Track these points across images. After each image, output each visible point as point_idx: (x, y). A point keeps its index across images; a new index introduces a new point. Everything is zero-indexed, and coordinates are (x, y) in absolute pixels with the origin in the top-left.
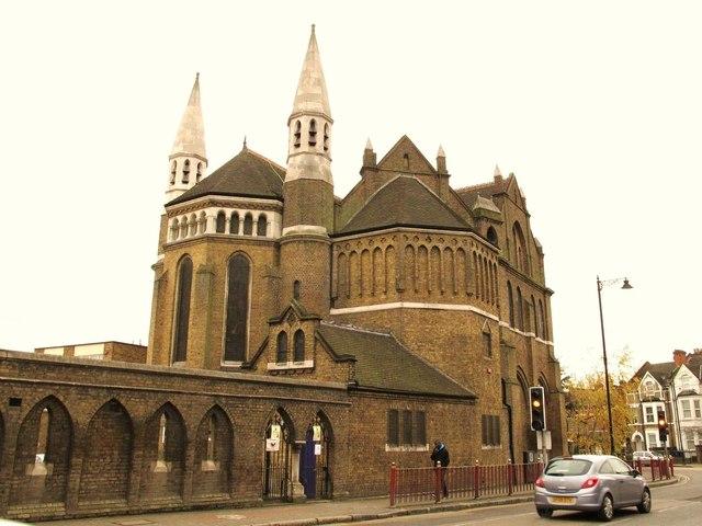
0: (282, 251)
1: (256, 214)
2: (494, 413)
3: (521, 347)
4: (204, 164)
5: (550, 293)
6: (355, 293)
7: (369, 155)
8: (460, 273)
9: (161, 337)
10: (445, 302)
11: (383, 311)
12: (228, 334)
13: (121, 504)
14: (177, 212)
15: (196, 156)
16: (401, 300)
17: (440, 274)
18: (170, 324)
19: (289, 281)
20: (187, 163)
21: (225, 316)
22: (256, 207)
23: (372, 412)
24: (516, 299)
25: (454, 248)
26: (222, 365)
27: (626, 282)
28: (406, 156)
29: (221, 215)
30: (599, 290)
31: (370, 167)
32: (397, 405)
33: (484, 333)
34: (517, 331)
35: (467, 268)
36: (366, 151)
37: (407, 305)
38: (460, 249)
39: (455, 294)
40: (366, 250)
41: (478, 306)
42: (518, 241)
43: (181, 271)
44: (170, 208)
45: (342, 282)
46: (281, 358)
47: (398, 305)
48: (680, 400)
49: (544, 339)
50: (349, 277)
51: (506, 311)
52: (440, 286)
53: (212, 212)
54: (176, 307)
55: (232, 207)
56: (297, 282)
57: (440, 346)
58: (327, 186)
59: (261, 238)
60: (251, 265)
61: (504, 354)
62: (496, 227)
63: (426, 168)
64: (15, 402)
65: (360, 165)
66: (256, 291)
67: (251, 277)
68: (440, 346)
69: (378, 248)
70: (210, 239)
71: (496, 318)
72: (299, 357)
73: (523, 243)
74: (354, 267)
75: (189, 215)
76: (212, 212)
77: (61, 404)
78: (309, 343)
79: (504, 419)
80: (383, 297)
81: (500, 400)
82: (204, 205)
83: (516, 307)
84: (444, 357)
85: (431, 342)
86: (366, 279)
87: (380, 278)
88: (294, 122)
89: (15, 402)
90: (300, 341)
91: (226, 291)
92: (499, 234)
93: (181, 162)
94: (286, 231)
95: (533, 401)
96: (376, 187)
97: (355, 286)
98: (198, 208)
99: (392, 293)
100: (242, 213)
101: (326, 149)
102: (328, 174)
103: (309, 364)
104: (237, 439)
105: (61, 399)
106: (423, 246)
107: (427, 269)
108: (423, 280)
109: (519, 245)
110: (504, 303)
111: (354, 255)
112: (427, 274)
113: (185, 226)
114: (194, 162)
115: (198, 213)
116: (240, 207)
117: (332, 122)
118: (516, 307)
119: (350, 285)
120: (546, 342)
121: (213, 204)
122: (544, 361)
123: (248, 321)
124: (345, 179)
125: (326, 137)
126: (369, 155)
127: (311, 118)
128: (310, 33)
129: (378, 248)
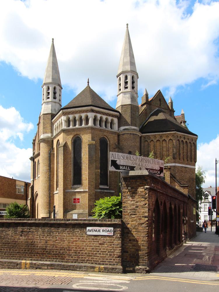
16: (175, 162)
30: (216, 164)
37: (177, 165)
40: (158, 140)
47: (173, 164)
53: (91, 115)
55: (100, 114)
60: (108, 143)
63: (166, 107)
69: (164, 140)
70: (92, 128)
76: (91, 115)
82: (87, 111)
85: (184, 180)
93: (122, 77)
94: (122, 128)
96: (150, 112)
101: (60, 100)
116: (104, 115)
121: (93, 111)
127: (47, 85)
128: (51, 43)
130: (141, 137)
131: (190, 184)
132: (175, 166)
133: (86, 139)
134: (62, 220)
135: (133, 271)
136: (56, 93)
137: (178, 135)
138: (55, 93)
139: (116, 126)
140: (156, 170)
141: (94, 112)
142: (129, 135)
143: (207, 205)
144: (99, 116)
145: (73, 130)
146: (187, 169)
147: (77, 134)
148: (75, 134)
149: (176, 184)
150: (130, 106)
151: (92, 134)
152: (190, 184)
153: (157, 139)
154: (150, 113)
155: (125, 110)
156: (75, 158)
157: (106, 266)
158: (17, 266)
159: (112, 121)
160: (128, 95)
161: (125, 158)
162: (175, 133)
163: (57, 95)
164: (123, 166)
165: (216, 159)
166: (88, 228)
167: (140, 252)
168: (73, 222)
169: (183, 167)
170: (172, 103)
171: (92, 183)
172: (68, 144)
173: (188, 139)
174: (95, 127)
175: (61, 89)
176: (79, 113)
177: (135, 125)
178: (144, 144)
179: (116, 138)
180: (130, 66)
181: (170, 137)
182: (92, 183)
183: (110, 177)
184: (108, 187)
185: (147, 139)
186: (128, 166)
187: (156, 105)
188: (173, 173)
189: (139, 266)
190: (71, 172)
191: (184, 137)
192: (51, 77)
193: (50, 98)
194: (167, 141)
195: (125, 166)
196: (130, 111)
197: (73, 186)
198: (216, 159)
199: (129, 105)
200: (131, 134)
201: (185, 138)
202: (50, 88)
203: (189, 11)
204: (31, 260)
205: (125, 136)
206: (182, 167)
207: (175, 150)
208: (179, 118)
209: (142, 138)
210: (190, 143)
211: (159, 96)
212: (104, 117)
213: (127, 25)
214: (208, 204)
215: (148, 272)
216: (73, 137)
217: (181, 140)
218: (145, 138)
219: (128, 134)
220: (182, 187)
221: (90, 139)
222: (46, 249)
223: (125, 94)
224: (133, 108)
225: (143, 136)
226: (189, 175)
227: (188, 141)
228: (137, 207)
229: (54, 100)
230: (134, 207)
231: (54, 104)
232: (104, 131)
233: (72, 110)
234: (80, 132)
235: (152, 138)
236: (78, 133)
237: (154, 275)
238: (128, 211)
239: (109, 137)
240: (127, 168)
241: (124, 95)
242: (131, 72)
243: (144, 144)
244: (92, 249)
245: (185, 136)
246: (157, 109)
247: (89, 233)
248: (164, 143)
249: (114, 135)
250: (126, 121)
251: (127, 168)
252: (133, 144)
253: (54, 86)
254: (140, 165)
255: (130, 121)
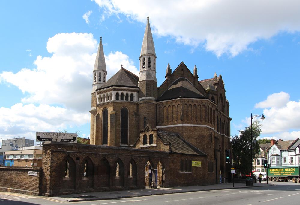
0: (139, 106)
1: (130, 93)
2: (212, 161)
3: (220, 139)
4: (106, 73)
5: (231, 119)
6: (165, 121)
7: (169, 70)
8: (203, 114)
9: (98, 136)
10: (197, 124)
11: (176, 127)
12: (121, 135)
13: (108, 188)
14: (101, 93)
15: (103, 71)
16: (183, 123)
17: (196, 114)
18: (101, 132)
19: (142, 117)
20: (100, 73)
21: (120, 129)
22: (129, 91)
23: (176, 161)
24: (219, 122)
25: (201, 105)
26: (120, 145)
27: (263, 116)
28: (183, 70)
29: (117, 94)
30: (252, 119)
31: (169, 74)
32: (183, 158)
33: (210, 134)
34: (219, 133)
35: (206, 112)
36: (168, 68)
37: (184, 125)
38: (204, 105)
39: (201, 121)
40: (169, 106)
41: (210, 126)
42: (221, 101)
43: (103, 113)
44: (98, 91)
45: (161, 117)
46: (145, 143)
47: (181, 125)
48: (271, 157)
49: (227, 136)
50: (163, 116)
51: (216, 127)
52: (196, 119)
53: (114, 93)
54: (102, 126)
56: (145, 117)
57: (195, 139)
58: (155, 83)
59: (132, 102)
60: (129, 111)
61: (216, 142)
62: (215, 96)
64: (78, 159)
65: (165, 74)
66: (130, 120)
67: (129, 117)
68: (195, 139)
69: (174, 105)
70: (114, 102)
71: (214, 129)
72: (151, 143)
73: (222, 102)
74: (165, 111)
75: (105, 94)
76: (114, 93)
77: (90, 159)
78: (155, 138)
79: (215, 163)
80: (176, 122)
81: (214, 157)
82: (111, 90)
83: (219, 125)
84: (196, 142)
86: (170, 116)
87: (175, 116)
88: (142, 59)
89: (78, 159)
90: (152, 138)
91: (120, 120)
92: (215, 99)
94: (140, 99)
95: (227, 157)
97: (165, 118)
98: (109, 91)
99: (180, 121)
100: (125, 93)
102: (155, 78)
103: (155, 145)
104: (138, 169)
105: (90, 157)
106: (195, 105)
107: (191, 112)
108: (190, 117)
109: (221, 102)
110: (216, 124)
111: (165, 108)
112: (192, 114)
113: (104, 98)
114: (102, 73)
115: (109, 93)
117: (156, 57)
118: (219, 125)
119: (164, 118)
120: (228, 137)
121: (114, 90)
122: (227, 143)
123: (128, 131)
124: (161, 79)
125: (154, 64)
126: (169, 70)
129: (174, 105)
130: (157, 104)
131: (200, 140)
132: (182, 127)
133: (110, 110)
134: (32, 168)
135: (44, 196)
136: (151, 62)
137: (185, 100)
138: (149, 62)
139: (135, 99)
140: (70, 140)
141: (116, 90)
142: (144, 104)
143: (275, 158)
144: (120, 92)
145: (103, 104)
146: (196, 128)
147: (105, 108)
148: (104, 107)
149: (161, 142)
150: (146, 82)
151: (114, 106)
152: (200, 140)
153: (169, 105)
154: (171, 83)
155: (142, 85)
156: (104, 124)
157: (33, 192)
158: (6, 191)
159: (132, 95)
160: (145, 73)
161: (46, 135)
162: (182, 99)
163: (152, 64)
164: (44, 139)
165: (252, 115)
166: (29, 172)
167: (47, 185)
168: (14, 168)
169: (192, 126)
170: (196, 71)
171: (113, 143)
172: (100, 115)
173: (197, 102)
174: (117, 101)
175: (106, 73)
176: (107, 92)
177: (150, 95)
178: (159, 110)
179: (135, 107)
180: (146, 50)
181: (179, 103)
182: (113, 143)
183: (129, 137)
184: (128, 145)
185: (161, 106)
186: (47, 139)
187: (179, 75)
188: (181, 132)
189: (47, 192)
190: (101, 135)
191: (193, 101)
192: (97, 66)
193: (97, 81)
194: (176, 106)
195: (46, 139)
196: (145, 86)
197: (103, 144)
198: (252, 115)
199: (146, 80)
200: (146, 103)
201: (193, 102)
202: (146, 59)
203: (36, 67)
204: (11, 188)
205: (142, 105)
206: (190, 126)
207: (182, 113)
208: (205, 82)
209: (158, 105)
210: (199, 105)
211: (182, 67)
212: (125, 93)
213: (101, 38)
214: (275, 157)
215: (50, 196)
216: (103, 110)
217: (188, 104)
218: (160, 105)
219: (144, 103)
220: (165, 144)
221: (113, 111)
222: (16, 182)
223: (143, 73)
224: (151, 83)
225: (158, 103)
226: (199, 133)
227: (197, 104)
228: (47, 161)
229: (100, 82)
230: (46, 161)
231: (99, 85)
232: (125, 103)
233: (102, 90)
234: (107, 106)
235: (165, 104)
236: (105, 106)
237: (51, 198)
238: (44, 163)
239: (129, 107)
240: (47, 140)
241: (142, 73)
242: (147, 55)
243: (159, 110)
244: (30, 183)
245: (194, 100)
246: (179, 78)
247: (29, 174)
248: (174, 107)
249: (133, 105)
250: (143, 93)
251: (47, 140)
252: (148, 111)
253: (99, 72)
254: (57, 137)
255: (145, 93)
